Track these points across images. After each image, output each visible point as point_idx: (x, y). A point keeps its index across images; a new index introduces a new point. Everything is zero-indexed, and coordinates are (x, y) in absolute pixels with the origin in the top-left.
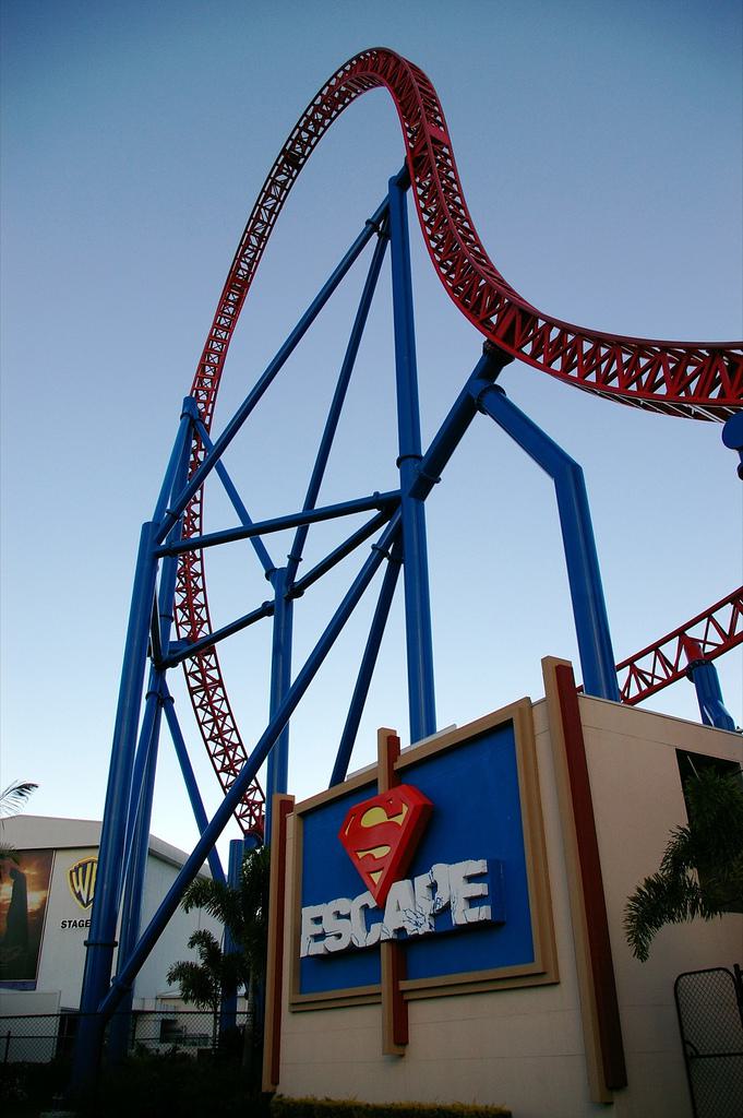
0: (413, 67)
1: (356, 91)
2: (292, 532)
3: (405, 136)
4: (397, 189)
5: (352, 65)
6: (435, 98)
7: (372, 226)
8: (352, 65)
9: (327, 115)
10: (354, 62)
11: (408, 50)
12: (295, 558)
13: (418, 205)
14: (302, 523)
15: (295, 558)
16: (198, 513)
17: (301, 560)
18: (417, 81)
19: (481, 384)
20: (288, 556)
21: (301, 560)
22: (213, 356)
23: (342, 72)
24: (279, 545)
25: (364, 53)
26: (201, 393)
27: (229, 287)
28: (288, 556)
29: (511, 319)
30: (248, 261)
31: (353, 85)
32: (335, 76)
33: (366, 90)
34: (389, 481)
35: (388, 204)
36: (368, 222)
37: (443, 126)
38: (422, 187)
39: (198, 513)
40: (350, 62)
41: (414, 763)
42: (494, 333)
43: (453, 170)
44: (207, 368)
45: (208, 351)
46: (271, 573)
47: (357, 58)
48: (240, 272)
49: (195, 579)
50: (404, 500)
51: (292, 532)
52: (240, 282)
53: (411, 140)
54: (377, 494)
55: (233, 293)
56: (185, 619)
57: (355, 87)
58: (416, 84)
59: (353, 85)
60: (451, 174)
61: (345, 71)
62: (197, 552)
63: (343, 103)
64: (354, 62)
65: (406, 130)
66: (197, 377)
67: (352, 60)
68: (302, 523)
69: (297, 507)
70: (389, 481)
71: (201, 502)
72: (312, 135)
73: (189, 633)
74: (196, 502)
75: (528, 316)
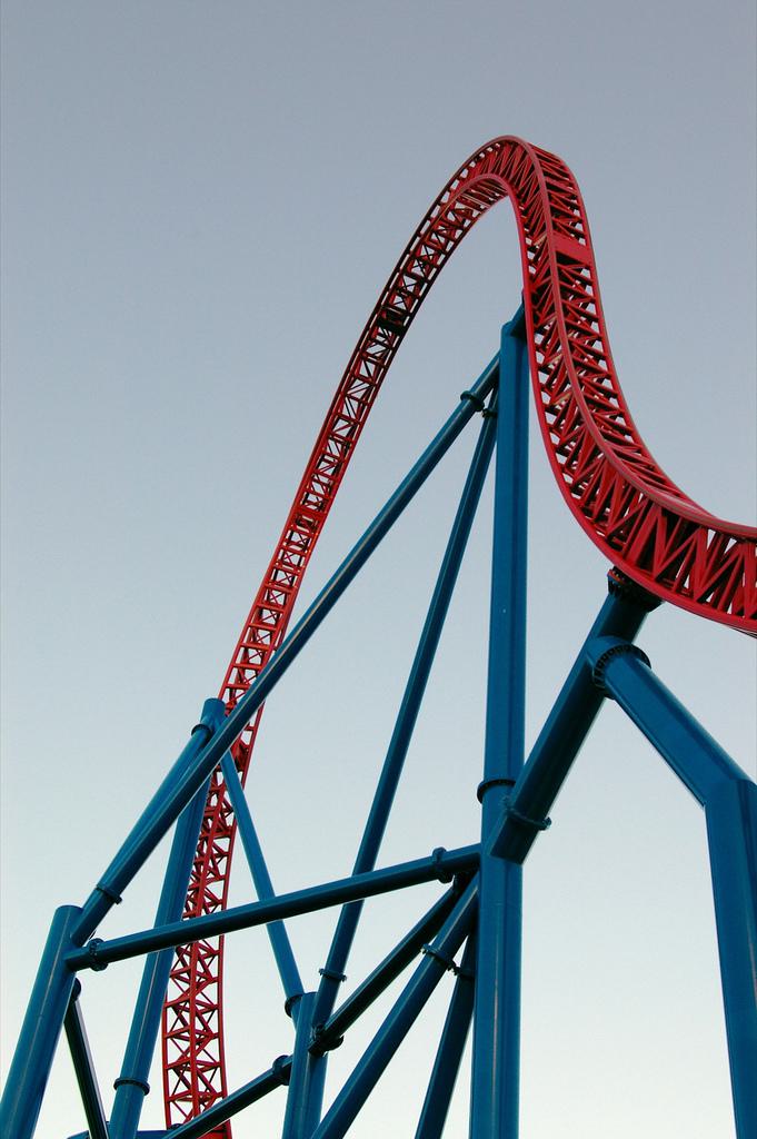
0: (547, 159)
1: (478, 208)
2: (333, 914)
3: (524, 256)
4: (512, 340)
5: (470, 169)
6: (567, 176)
7: (472, 402)
8: (470, 169)
9: (440, 250)
10: (473, 165)
11: (536, 135)
12: (333, 975)
13: (542, 419)
14: (349, 896)
15: (333, 975)
16: (226, 850)
17: (344, 978)
18: (546, 174)
19: (605, 645)
20: (321, 971)
21: (344, 978)
22: (275, 593)
23: (457, 236)
24: (312, 935)
25: (484, 150)
26: (252, 652)
27: (295, 520)
28: (321, 971)
29: (649, 529)
30: (325, 480)
31: (471, 199)
32: (448, 188)
33: (491, 203)
34: (463, 827)
35: (498, 367)
36: (464, 396)
37: (615, 396)
38: (565, 453)
39: (220, 897)
40: (466, 166)
41: (431, 470)
42: (624, 557)
43: (609, 377)
44: (266, 613)
45: (269, 584)
46: (295, 1000)
47: (476, 157)
48: (312, 498)
49: (207, 961)
50: (484, 862)
51: (333, 914)
52: (310, 514)
53: (567, 468)
54: (440, 852)
55: (300, 533)
56: (182, 1088)
57: (477, 201)
58: (542, 179)
59: (471, 199)
60: (607, 384)
61: (462, 180)
62: (213, 942)
63: (461, 228)
64: (473, 165)
65: (526, 248)
66: (248, 626)
67: (469, 161)
68: (349, 896)
69: (342, 868)
70: (463, 827)
71: (226, 878)
72: (420, 281)
73: (188, 1118)
74: (218, 877)
75: (685, 526)
